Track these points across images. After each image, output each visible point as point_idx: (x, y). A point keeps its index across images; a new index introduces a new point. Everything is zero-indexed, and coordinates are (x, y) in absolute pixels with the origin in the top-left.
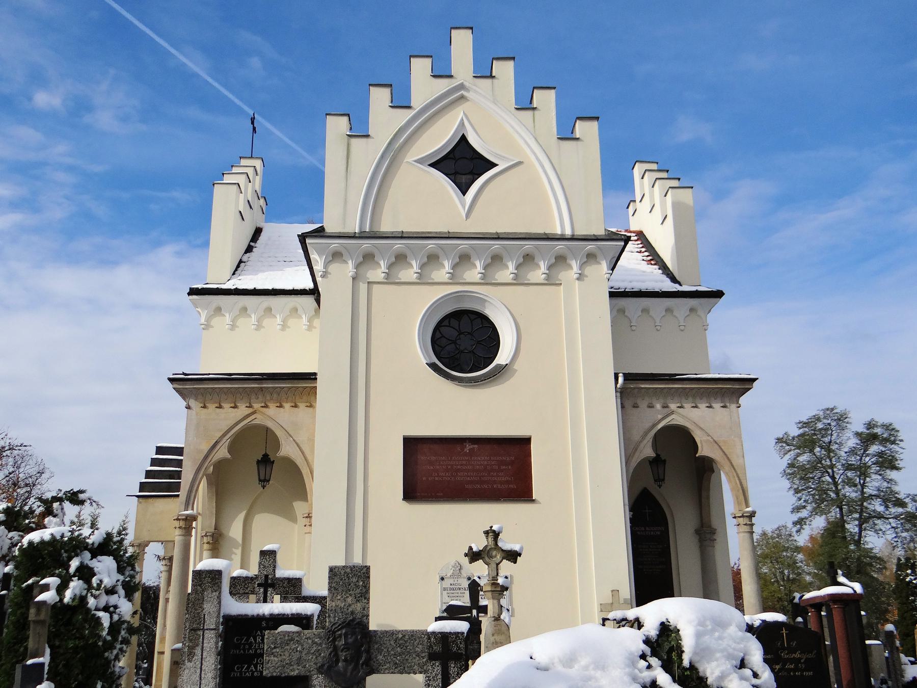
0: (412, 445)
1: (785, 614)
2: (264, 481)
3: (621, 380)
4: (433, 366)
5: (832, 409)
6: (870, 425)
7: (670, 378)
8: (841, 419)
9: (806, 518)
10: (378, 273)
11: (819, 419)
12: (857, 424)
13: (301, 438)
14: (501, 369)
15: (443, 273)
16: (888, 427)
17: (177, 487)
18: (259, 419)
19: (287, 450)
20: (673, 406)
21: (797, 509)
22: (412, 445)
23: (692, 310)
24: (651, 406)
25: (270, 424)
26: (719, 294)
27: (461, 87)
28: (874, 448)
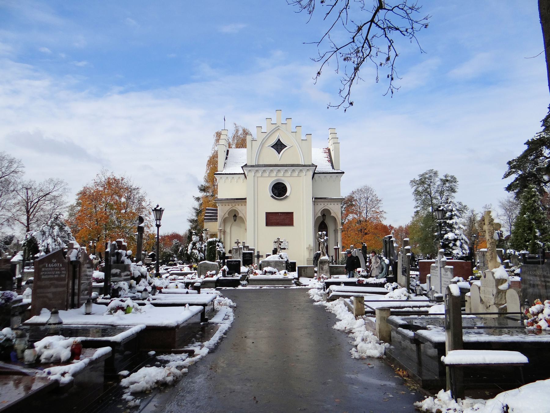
0: (268, 214)
1: (120, 269)
2: (235, 220)
3: (314, 199)
4: (272, 196)
5: (432, 170)
6: (446, 176)
7: (325, 198)
8: (436, 173)
9: (419, 210)
10: (259, 174)
11: (427, 174)
12: (441, 176)
13: (244, 212)
14: (287, 197)
15: (274, 174)
16: (452, 177)
17: (217, 219)
18: (234, 208)
19: (240, 215)
20: (326, 204)
21: (417, 207)
22: (268, 214)
23: (337, 176)
24: (321, 204)
25: (236, 209)
26: (343, 173)
27: (279, 126)
28: (447, 184)
